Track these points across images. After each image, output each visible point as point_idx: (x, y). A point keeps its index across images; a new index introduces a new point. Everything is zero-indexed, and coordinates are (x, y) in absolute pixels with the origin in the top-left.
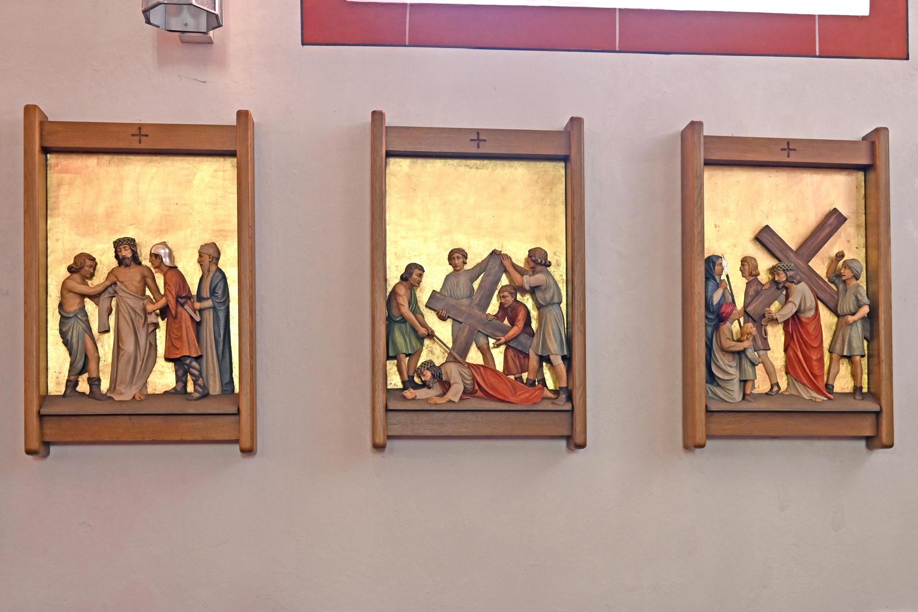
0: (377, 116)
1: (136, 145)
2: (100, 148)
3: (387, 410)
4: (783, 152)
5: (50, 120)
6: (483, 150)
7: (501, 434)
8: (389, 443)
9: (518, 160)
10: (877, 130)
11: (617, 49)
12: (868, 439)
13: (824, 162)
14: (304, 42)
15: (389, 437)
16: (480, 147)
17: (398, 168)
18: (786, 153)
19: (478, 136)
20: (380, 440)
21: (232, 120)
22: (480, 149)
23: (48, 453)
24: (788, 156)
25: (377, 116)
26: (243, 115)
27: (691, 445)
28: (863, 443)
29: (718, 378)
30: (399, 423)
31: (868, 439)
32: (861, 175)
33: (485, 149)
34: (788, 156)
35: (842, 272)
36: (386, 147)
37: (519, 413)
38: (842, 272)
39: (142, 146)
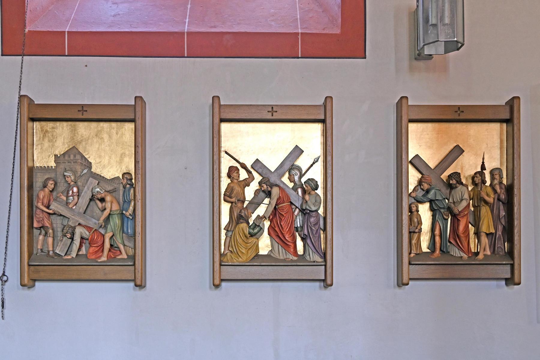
0: (216, 98)
1: (80, 116)
2: (60, 118)
3: (29, 265)
4: (79, 112)
5: (36, 103)
6: (462, 117)
7: (119, 278)
8: (224, 284)
10: (514, 98)
11: (66, 54)
12: (506, 280)
13: (93, 117)
14: (4, 54)
15: (222, 280)
16: (460, 116)
17: (225, 127)
18: (270, 114)
19: (272, 109)
20: (217, 282)
21: (321, 102)
22: (83, 116)
23: (34, 286)
24: (83, 115)
25: (216, 98)
26: (328, 99)
27: (217, 286)
28: (503, 282)
29: (239, 246)
30: (228, 272)
31: (506, 280)
32: (505, 125)
33: (276, 116)
34: (83, 115)
35: (451, 182)
36: (408, 115)
37: (443, 266)
38: (451, 182)
39: (274, 117)
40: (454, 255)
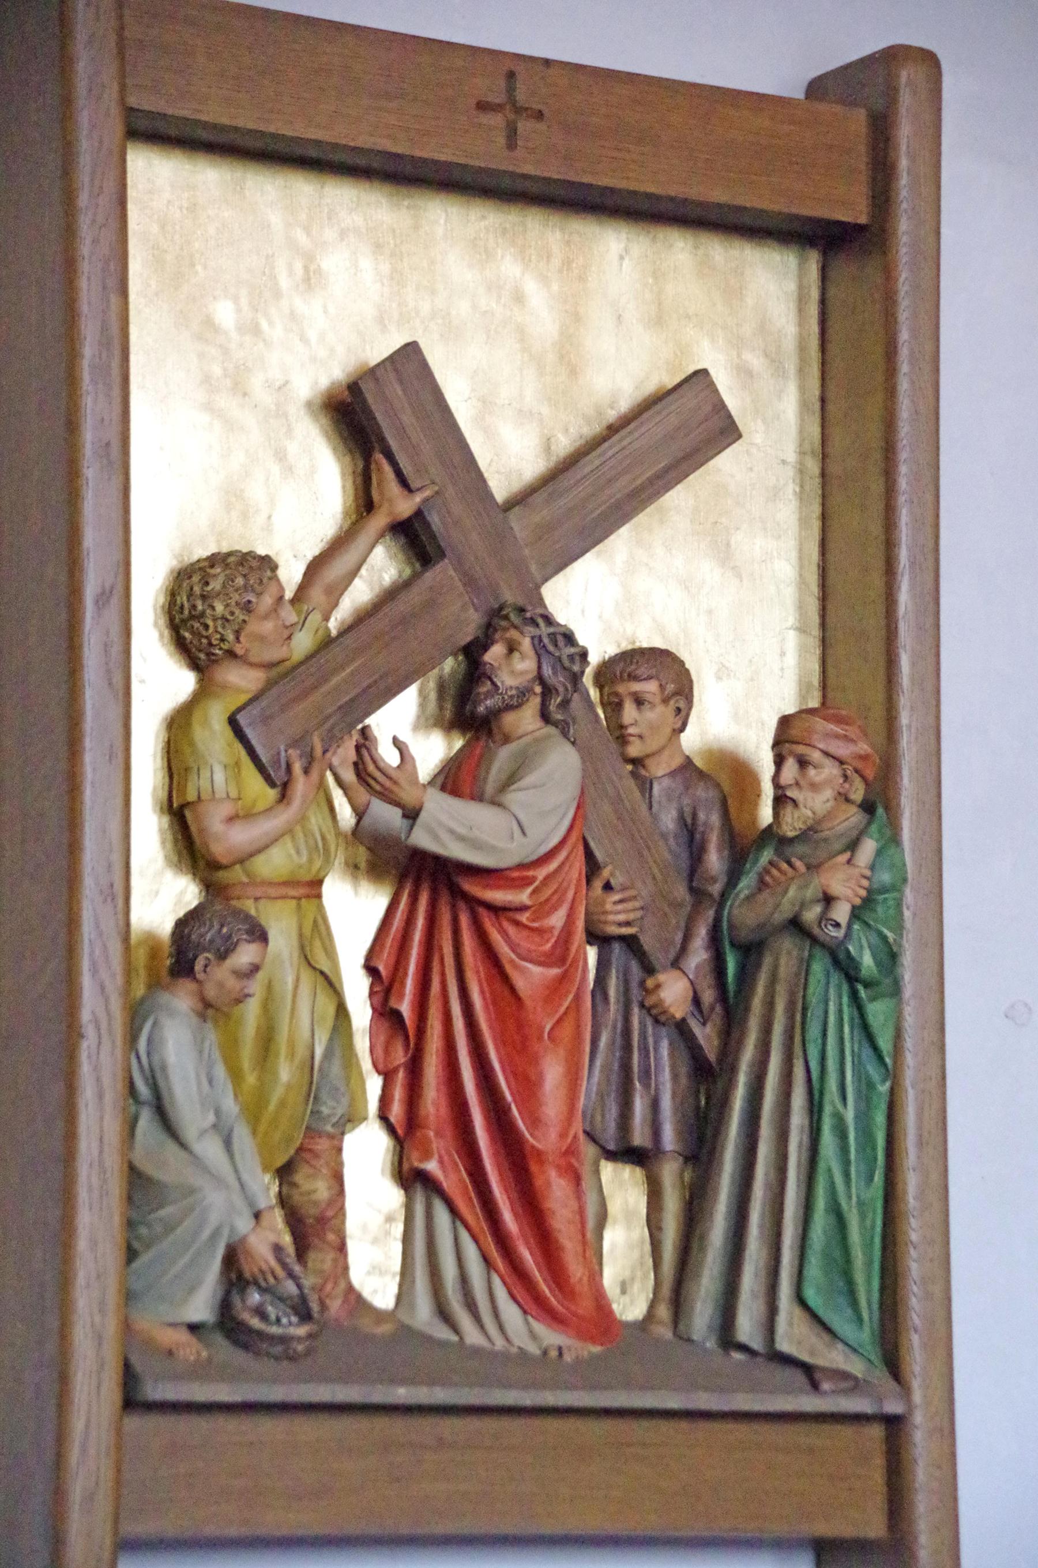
9: (388, 188)
40: (499, 1343)
